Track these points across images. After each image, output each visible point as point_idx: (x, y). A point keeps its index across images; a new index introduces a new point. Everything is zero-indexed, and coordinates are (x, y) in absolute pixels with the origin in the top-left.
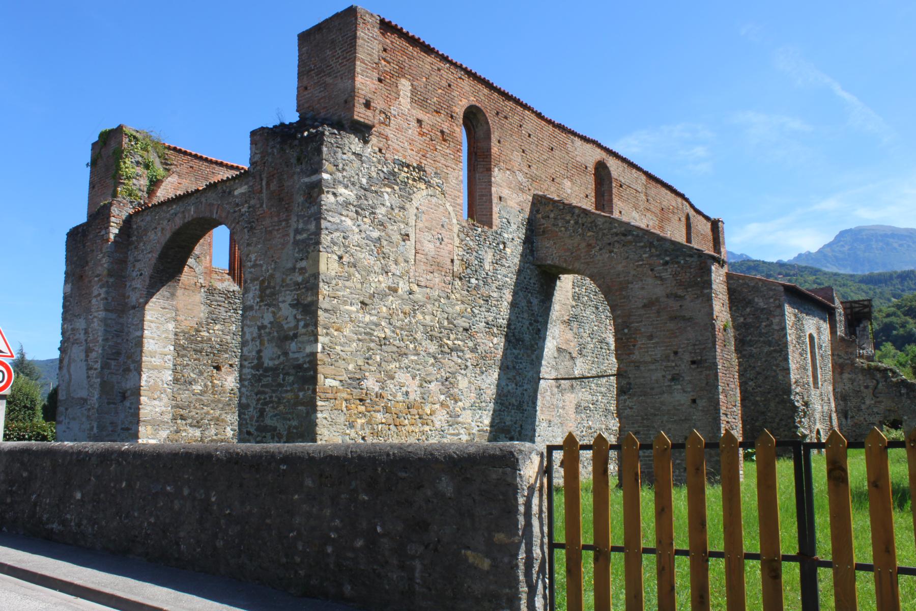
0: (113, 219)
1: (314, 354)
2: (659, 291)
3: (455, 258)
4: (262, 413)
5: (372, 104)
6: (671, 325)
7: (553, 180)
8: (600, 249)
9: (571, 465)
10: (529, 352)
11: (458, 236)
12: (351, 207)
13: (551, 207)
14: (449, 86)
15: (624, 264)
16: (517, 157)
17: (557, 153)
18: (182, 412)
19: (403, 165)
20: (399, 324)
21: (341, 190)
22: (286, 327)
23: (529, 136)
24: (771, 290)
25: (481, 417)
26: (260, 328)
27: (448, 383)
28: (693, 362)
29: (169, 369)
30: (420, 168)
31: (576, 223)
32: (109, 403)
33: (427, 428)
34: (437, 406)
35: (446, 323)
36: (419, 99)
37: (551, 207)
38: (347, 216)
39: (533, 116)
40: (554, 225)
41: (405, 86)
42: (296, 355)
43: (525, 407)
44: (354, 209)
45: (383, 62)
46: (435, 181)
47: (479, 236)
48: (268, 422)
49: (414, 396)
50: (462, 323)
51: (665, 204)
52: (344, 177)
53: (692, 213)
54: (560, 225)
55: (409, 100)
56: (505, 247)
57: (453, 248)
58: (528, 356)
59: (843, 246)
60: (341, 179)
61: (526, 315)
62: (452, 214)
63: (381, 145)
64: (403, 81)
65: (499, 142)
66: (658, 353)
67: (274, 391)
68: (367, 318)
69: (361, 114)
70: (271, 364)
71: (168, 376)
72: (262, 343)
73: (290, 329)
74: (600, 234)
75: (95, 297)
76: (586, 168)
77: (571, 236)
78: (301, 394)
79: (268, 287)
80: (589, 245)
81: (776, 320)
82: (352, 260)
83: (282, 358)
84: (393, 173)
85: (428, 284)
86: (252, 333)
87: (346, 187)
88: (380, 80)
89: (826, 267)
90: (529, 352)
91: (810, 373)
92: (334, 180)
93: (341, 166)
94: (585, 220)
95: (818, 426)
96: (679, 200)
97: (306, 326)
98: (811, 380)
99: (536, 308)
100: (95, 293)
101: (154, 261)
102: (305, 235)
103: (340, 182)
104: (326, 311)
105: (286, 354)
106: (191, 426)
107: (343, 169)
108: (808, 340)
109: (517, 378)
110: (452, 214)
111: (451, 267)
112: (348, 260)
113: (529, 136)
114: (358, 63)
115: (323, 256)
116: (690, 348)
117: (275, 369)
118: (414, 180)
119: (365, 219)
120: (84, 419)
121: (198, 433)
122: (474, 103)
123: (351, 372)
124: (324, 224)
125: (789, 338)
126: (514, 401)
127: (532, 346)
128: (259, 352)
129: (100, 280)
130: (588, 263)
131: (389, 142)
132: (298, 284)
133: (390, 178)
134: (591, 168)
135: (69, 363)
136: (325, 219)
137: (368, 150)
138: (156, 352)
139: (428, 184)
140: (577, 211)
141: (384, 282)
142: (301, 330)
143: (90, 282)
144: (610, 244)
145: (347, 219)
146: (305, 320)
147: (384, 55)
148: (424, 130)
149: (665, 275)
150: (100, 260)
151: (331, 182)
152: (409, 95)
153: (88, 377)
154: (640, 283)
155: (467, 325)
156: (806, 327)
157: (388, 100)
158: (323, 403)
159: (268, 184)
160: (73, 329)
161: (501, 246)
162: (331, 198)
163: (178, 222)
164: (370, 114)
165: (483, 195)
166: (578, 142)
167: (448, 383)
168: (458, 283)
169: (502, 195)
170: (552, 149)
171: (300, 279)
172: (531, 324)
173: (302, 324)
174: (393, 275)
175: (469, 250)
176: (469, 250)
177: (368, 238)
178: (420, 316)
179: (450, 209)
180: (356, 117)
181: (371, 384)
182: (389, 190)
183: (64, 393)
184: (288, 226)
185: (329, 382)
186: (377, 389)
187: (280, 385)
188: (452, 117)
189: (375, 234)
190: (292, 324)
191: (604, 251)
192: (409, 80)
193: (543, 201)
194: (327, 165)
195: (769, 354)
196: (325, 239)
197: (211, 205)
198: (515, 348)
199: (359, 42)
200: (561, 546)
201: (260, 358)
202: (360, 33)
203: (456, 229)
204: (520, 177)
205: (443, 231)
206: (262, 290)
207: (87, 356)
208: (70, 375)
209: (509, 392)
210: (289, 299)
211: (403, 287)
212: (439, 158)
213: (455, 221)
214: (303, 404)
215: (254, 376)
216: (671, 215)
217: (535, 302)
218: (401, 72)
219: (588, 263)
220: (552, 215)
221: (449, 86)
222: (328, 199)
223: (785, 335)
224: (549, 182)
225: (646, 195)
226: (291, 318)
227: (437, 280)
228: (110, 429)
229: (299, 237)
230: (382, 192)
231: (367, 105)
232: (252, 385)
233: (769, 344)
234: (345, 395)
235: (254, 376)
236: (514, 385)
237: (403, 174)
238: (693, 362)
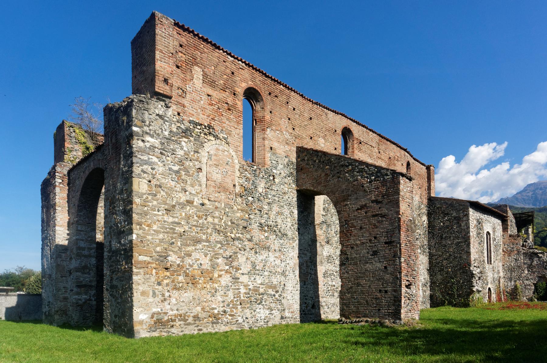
0: (57, 174)
1: (131, 241)
3: (237, 184)
5: (169, 81)
7: (311, 138)
8: (333, 176)
10: (291, 241)
11: (239, 170)
12: (157, 150)
13: (305, 153)
14: (233, 73)
15: (346, 184)
16: (284, 122)
17: (314, 121)
19: (196, 124)
20: (195, 223)
21: (148, 138)
23: (294, 109)
24: (462, 205)
25: (255, 279)
27: (230, 259)
29: (93, 257)
30: (209, 127)
31: (319, 162)
32: (62, 277)
33: (216, 285)
34: (223, 273)
35: (230, 223)
37: (305, 153)
38: (153, 155)
39: (297, 96)
40: (307, 164)
41: (197, 72)
43: (287, 273)
44: (159, 151)
46: (221, 136)
47: (255, 171)
50: (243, 223)
51: (392, 155)
52: (150, 130)
53: (412, 161)
54: (311, 164)
55: (201, 81)
56: (274, 178)
57: (236, 179)
58: (290, 244)
59: (528, 193)
60: (148, 131)
61: (289, 220)
62: (235, 157)
63: (180, 111)
64: (196, 68)
65: (271, 112)
68: (171, 220)
69: (160, 87)
72: (111, 237)
74: (333, 166)
76: (336, 131)
77: (316, 170)
80: (326, 174)
82: (158, 183)
84: (187, 129)
85: (216, 199)
87: (152, 136)
89: (517, 204)
91: (486, 255)
92: (143, 131)
93: (147, 123)
94: (324, 159)
95: (490, 286)
96: (403, 152)
98: (486, 259)
103: (147, 133)
104: (137, 214)
107: (150, 125)
108: (485, 235)
109: (282, 256)
110: (235, 157)
111: (233, 189)
112: (155, 183)
113: (294, 109)
114: (157, 52)
115: (135, 181)
118: (205, 134)
119: (168, 158)
122: (251, 86)
123: (158, 252)
124: (135, 160)
125: (471, 234)
126: (279, 270)
130: (325, 186)
131: (186, 109)
133: (186, 133)
134: (339, 131)
136: (136, 156)
137: (170, 112)
139: (216, 137)
140: (320, 154)
141: (183, 198)
144: (338, 173)
145: (153, 157)
147: (181, 49)
148: (213, 102)
151: (141, 133)
152: (201, 78)
154: (355, 196)
155: (245, 225)
156: (484, 227)
158: (138, 271)
161: (271, 178)
162: (141, 144)
163: (87, 173)
164: (168, 88)
165: (260, 147)
166: (331, 114)
167: (230, 259)
168: (239, 200)
169: (273, 146)
170: (311, 119)
174: (190, 193)
175: (248, 179)
176: (248, 179)
177: (170, 169)
178: (210, 219)
179: (233, 154)
180: (156, 90)
181: (173, 258)
185: (142, 258)
186: (178, 262)
188: (234, 94)
189: (176, 168)
191: (335, 177)
192: (201, 68)
193: (302, 150)
194: (136, 121)
196: (137, 169)
197: (99, 160)
198: (281, 239)
199: (158, 38)
202: (158, 31)
203: (237, 167)
204: (287, 136)
205: (228, 167)
209: (276, 265)
211: (197, 201)
212: (225, 120)
213: (236, 161)
215: (108, 256)
216: (396, 162)
218: (194, 62)
220: (306, 158)
221: (233, 73)
222: (137, 144)
223: (469, 232)
224: (308, 139)
225: (379, 149)
227: (223, 197)
228: (64, 291)
230: (181, 141)
231: (166, 81)
232: (108, 262)
234: (154, 265)
235: (108, 256)
236: (279, 261)
237: (197, 130)
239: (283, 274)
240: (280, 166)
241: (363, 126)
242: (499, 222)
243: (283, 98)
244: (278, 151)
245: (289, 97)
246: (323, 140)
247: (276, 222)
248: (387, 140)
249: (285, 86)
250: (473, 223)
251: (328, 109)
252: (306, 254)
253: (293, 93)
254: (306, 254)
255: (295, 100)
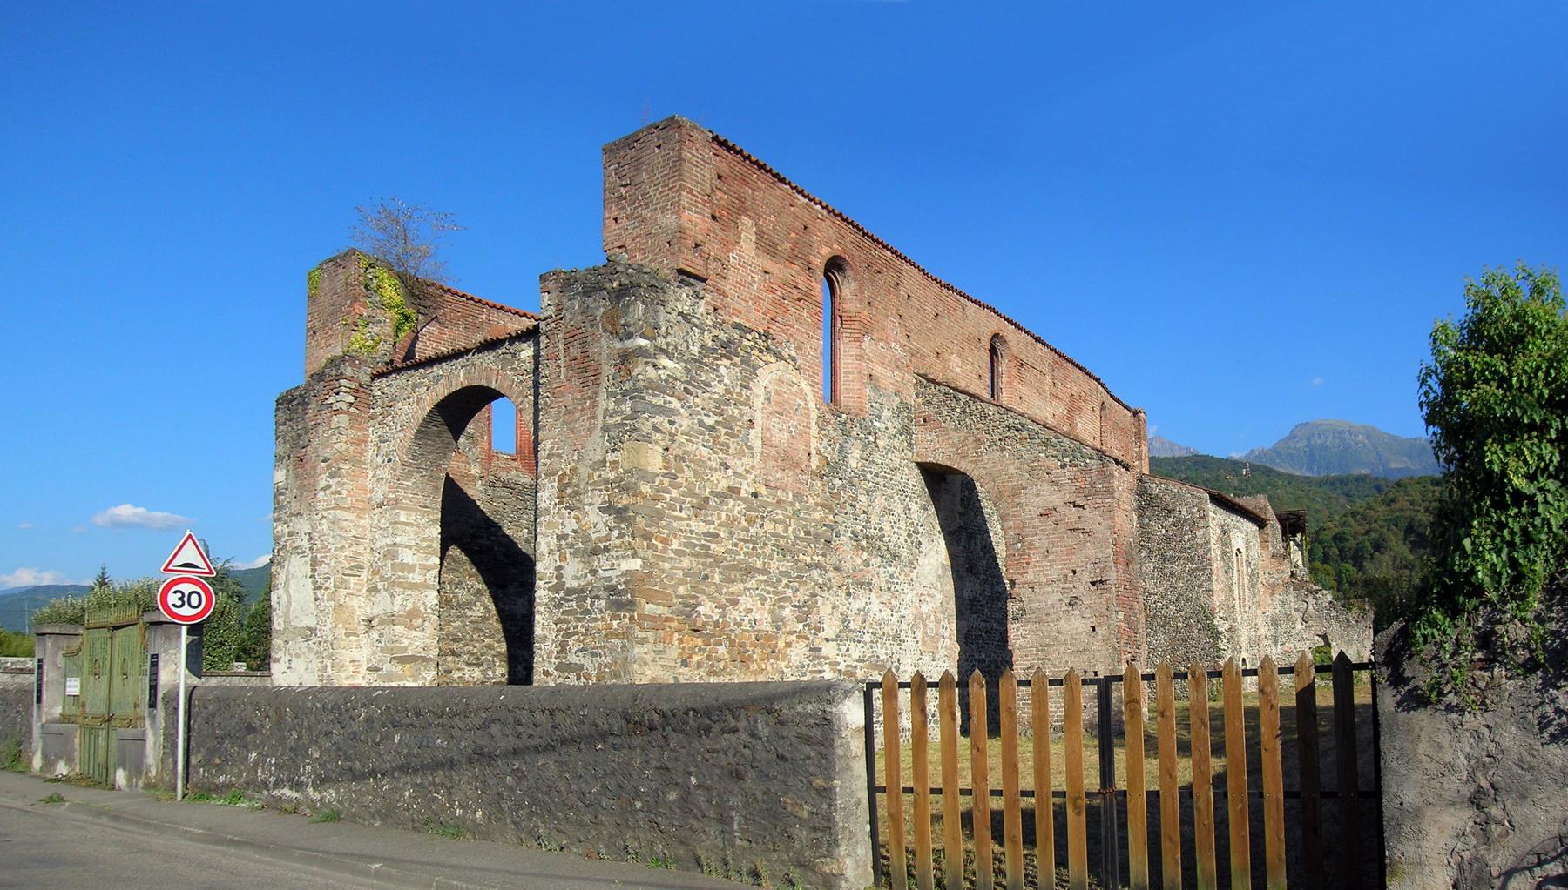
2: (1055, 499)
4: (563, 647)
6: (1069, 541)
9: (890, 697)
10: (907, 570)
17: (945, 321)
18: (454, 646)
21: (664, 361)
22: (594, 536)
26: (559, 538)
27: (805, 610)
28: (1093, 584)
30: (767, 336)
31: (963, 412)
36: (767, 246)
42: (607, 574)
45: (719, 194)
48: (572, 658)
49: (766, 626)
61: (902, 524)
64: (745, 219)
66: (1054, 572)
67: (579, 620)
70: (575, 584)
71: (432, 597)
72: (563, 558)
73: (600, 540)
75: (324, 489)
78: (615, 623)
79: (569, 485)
80: (977, 440)
81: (1199, 534)
83: (589, 577)
86: (548, 544)
88: (714, 218)
90: (907, 570)
97: (620, 536)
99: (915, 516)
100: (323, 484)
101: (407, 443)
102: (619, 419)
103: (662, 350)
105: (594, 572)
106: (468, 664)
116: (1089, 567)
117: (580, 591)
118: (761, 351)
120: (312, 656)
121: (477, 674)
127: (911, 563)
128: (559, 568)
129: (329, 467)
130: (975, 462)
132: (606, 481)
133: (727, 348)
134: (986, 343)
135: (287, 580)
137: (702, 308)
138: (414, 566)
142: (615, 542)
143: (314, 468)
146: (620, 529)
147: (718, 183)
149: (1064, 480)
150: (328, 438)
151: (652, 350)
153: (316, 599)
157: (727, 245)
159: (567, 350)
160: (290, 534)
161: (871, 438)
171: (612, 475)
172: (909, 536)
173: (615, 533)
181: (706, 609)
182: (727, 362)
183: (281, 620)
184: (595, 405)
187: (587, 612)
190: (604, 533)
195: (1191, 573)
200: (883, 790)
201: (559, 577)
204: (899, 352)
206: (562, 488)
207: (314, 571)
208: (289, 596)
210: (598, 500)
214: (617, 636)
217: (915, 507)
219: (975, 462)
224: (933, 358)
226: (601, 526)
229: (611, 421)
232: (550, 612)
233: (1192, 561)
238: (1093, 584)
239: (896, 638)
240: (886, 414)
241: (1027, 333)
242: (1255, 528)
243: (889, 277)
244: (883, 383)
245: (899, 272)
246: (957, 360)
247: (881, 529)
248: (1068, 360)
249: (894, 252)
250: (1214, 532)
251: (967, 298)
252: (933, 596)
253: (907, 267)
254: (933, 596)
255: (911, 278)
